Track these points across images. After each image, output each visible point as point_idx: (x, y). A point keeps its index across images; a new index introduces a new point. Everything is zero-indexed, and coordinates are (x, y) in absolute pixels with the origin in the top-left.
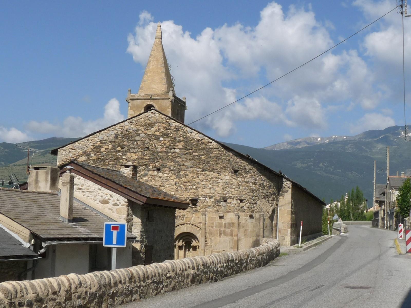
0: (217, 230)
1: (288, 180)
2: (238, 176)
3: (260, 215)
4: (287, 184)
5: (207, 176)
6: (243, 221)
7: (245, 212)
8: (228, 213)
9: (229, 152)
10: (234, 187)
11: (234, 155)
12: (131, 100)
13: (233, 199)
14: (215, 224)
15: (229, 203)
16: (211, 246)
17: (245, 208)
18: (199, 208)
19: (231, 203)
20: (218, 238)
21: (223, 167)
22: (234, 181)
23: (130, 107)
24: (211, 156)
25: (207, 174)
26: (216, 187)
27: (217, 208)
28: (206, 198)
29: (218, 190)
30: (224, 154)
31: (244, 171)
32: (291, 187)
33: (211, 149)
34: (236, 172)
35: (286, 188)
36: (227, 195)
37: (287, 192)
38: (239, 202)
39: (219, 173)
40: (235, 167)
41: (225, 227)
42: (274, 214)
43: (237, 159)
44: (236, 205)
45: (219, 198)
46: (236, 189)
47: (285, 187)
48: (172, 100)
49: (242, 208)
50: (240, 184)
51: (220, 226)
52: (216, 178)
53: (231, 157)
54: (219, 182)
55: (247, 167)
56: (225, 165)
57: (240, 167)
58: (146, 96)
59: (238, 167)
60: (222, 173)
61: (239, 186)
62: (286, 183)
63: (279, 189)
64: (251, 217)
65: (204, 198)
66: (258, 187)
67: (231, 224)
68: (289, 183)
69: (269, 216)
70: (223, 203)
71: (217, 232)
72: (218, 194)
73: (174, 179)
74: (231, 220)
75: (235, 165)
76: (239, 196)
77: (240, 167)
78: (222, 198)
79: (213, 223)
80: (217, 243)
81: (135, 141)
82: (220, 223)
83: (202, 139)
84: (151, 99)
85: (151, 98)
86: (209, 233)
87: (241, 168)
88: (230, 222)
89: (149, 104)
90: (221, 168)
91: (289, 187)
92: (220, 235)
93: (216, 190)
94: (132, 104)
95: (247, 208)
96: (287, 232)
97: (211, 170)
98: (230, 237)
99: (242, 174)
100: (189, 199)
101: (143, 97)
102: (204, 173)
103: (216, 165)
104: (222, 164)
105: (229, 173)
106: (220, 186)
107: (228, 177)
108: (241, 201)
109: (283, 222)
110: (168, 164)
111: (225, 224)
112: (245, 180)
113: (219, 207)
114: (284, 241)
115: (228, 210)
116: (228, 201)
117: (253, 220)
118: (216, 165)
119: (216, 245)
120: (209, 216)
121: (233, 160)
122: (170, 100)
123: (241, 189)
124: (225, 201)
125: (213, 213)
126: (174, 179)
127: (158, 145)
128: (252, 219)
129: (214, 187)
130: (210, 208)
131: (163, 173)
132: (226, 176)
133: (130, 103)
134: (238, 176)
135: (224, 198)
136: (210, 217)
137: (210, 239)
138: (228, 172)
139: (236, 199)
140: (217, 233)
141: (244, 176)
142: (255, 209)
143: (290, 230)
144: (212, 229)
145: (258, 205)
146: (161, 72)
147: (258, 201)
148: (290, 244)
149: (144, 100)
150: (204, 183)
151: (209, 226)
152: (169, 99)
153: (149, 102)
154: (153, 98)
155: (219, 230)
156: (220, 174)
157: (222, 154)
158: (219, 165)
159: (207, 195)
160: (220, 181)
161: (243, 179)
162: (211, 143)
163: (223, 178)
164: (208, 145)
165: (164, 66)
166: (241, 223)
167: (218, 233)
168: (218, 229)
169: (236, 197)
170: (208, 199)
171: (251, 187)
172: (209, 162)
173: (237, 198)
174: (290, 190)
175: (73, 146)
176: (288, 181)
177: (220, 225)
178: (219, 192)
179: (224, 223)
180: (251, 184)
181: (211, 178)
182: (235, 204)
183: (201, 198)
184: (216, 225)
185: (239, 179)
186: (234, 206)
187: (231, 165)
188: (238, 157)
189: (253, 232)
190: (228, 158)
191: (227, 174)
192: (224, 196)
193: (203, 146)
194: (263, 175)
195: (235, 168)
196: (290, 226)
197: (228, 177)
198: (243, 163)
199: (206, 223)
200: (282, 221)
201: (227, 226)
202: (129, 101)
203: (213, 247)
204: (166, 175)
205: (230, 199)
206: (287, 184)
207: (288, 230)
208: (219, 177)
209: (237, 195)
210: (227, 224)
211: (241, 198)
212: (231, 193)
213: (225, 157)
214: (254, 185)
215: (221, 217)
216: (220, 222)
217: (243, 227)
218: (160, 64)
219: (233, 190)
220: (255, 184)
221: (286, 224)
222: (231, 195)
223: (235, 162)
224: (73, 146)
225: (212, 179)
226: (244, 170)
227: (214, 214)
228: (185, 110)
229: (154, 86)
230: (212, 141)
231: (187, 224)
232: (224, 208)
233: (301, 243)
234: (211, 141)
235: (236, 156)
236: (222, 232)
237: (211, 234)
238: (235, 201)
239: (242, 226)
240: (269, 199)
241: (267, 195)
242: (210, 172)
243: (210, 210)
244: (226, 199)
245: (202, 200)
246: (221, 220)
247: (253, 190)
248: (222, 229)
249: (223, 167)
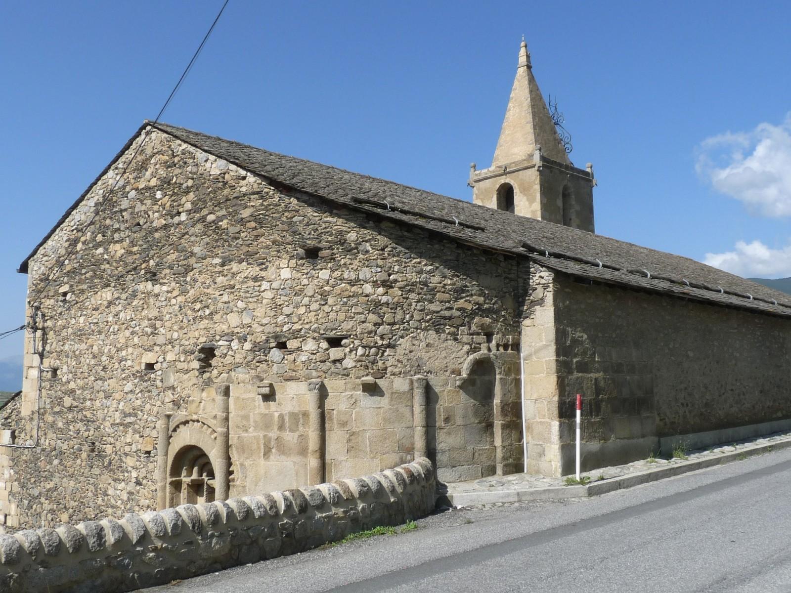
0: (257, 438)
1: (542, 266)
2: (319, 267)
3: (412, 382)
4: (542, 277)
5: (234, 275)
6: (343, 406)
7: (348, 376)
8: (289, 383)
9: (291, 197)
10: (306, 300)
11: (303, 204)
12: (475, 182)
13: (304, 339)
14: (252, 420)
15: (291, 352)
16: (244, 487)
17: (349, 363)
18: (215, 372)
19: (299, 349)
20: (262, 461)
21: (274, 242)
22: (305, 282)
23: (476, 194)
24: (243, 216)
25: (232, 271)
26: (255, 305)
27: (259, 369)
28: (231, 341)
29: (259, 314)
30: (276, 205)
31: (337, 250)
32: (551, 285)
33: (244, 195)
34: (312, 254)
35: (539, 293)
36: (285, 328)
37: (541, 302)
38: (324, 345)
39: (262, 264)
40: (309, 239)
41: (281, 427)
42: (495, 375)
43: (316, 214)
44: (314, 357)
45: (264, 338)
46: (315, 306)
47: (536, 289)
48: (540, 167)
49: (338, 365)
50: (326, 288)
51: (267, 426)
52: (256, 279)
53: (297, 211)
54: (262, 289)
55: (352, 236)
56: (278, 238)
57: (324, 236)
58: (499, 169)
59: (319, 239)
60: (270, 262)
61: (324, 296)
62: (538, 275)
63: (518, 302)
64: (372, 389)
65: (227, 341)
66: (400, 293)
67: (301, 416)
68: (547, 274)
69: (458, 383)
70: (276, 354)
71: (258, 444)
72: (261, 325)
73: (176, 296)
74: (299, 406)
75: (307, 232)
76: (324, 327)
77: (324, 236)
78: (272, 337)
79: (246, 417)
80: (260, 480)
81: (121, 211)
82: (266, 415)
83: (224, 174)
84: (505, 173)
85: (504, 170)
86: (237, 448)
87: (330, 239)
88: (296, 410)
89: (503, 182)
90: (267, 247)
91: (545, 287)
92: (267, 453)
93: (255, 314)
94: (478, 189)
95: (354, 364)
96: (550, 432)
97: (242, 256)
98: (297, 459)
99: (334, 259)
100: (198, 347)
101: (494, 172)
102: (226, 268)
103: (253, 240)
104: (270, 235)
105: (292, 257)
106: (265, 301)
107: (286, 273)
108: (335, 342)
109: (536, 400)
110: (168, 257)
111: (281, 417)
112: (346, 275)
113: (264, 366)
114: (543, 459)
115: (290, 373)
116: (292, 344)
117: (384, 402)
118: (253, 240)
119: (256, 486)
120: (237, 395)
121: (302, 218)
122: (536, 168)
123: (330, 306)
124: (282, 346)
125: (247, 385)
126: (176, 296)
127: (153, 213)
128: (376, 398)
129: (251, 306)
130: (239, 369)
131: (160, 284)
132: (282, 271)
133: (475, 188)
134: (319, 267)
135: (276, 337)
136: (238, 398)
137: (242, 465)
138: (288, 257)
139: (314, 338)
140: (259, 448)
141: (342, 262)
142: (388, 364)
143: (557, 423)
144: (246, 435)
145: (400, 350)
146: (527, 123)
147: (402, 337)
148: (560, 470)
149: (495, 179)
150: (225, 298)
151: (238, 427)
152: (534, 166)
153: (503, 180)
154: (508, 170)
155: (265, 436)
156: (264, 266)
157: (269, 205)
158: (262, 239)
159: (233, 332)
160: (265, 285)
161: (336, 273)
162: (244, 178)
163: (273, 277)
164: (236, 185)
165: (531, 111)
166: (335, 412)
167: (262, 447)
168: (261, 435)
169: (314, 331)
170: (235, 344)
171: (367, 296)
172: (237, 235)
173: (316, 335)
174: (549, 298)
175: (45, 249)
176: (544, 269)
177: (266, 422)
178: (265, 321)
179: (276, 414)
180: (368, 288)
181: (242, 282)
182: (312, 354)
183: (220, 343)
184: (255, 422)
185: (324, 274)
186: (310, 360)
187: (294, 233)
188: (315, 209)
189: (385, 439)
190: (286, 214)
191: (283, 263)
192: (278, 329)
193: (227, 191)
194: (421, 255)
195: (309, 242)
196: (556, 412)
197: (286, 273)
198: (337, 223)
199: (231, 415)
200: (535, 397)
201: (287, 425)
202: (472, 184)
203: (249, 489)
204: (165, 288)
205: (296, 338)
206: (541, 278)
207: (553, 423)
208: (263, 274)
209: (316, 325)
210: (287, 419)
211: (332, 334)
212: (295, 319)
213: (278, 213)
214: (381, 290)
215: (269, 397)
216: (267, 412)
217: (343, 424)
218: (525, 109)
219: (302, 310)
220: (387, 285)
221: (545, 403)
222: (297, 327)
223: (308, 224)
224: (45, 249)
225: (246, 282)
226: (342, 244)
227: (250, 387)
228: (593, 187)
229: (516, 150)
230: (245, 172)
231: (194, 421)
232: (279, 368)
233: (582, 471)
234: (243, 173)
235: (311, 205)
236: (273, 443)
237: (244, 451)
238: (310, 345)
239: (337, 420)
240: (457, 327)
241: (445, 318)
242: (240, 264)
243: (241, 375)
244: (284, 340)
245: (222, 348)
246: (269, 405)
247: (378, 304)
248: (273, 434)
249: (274, 242)
